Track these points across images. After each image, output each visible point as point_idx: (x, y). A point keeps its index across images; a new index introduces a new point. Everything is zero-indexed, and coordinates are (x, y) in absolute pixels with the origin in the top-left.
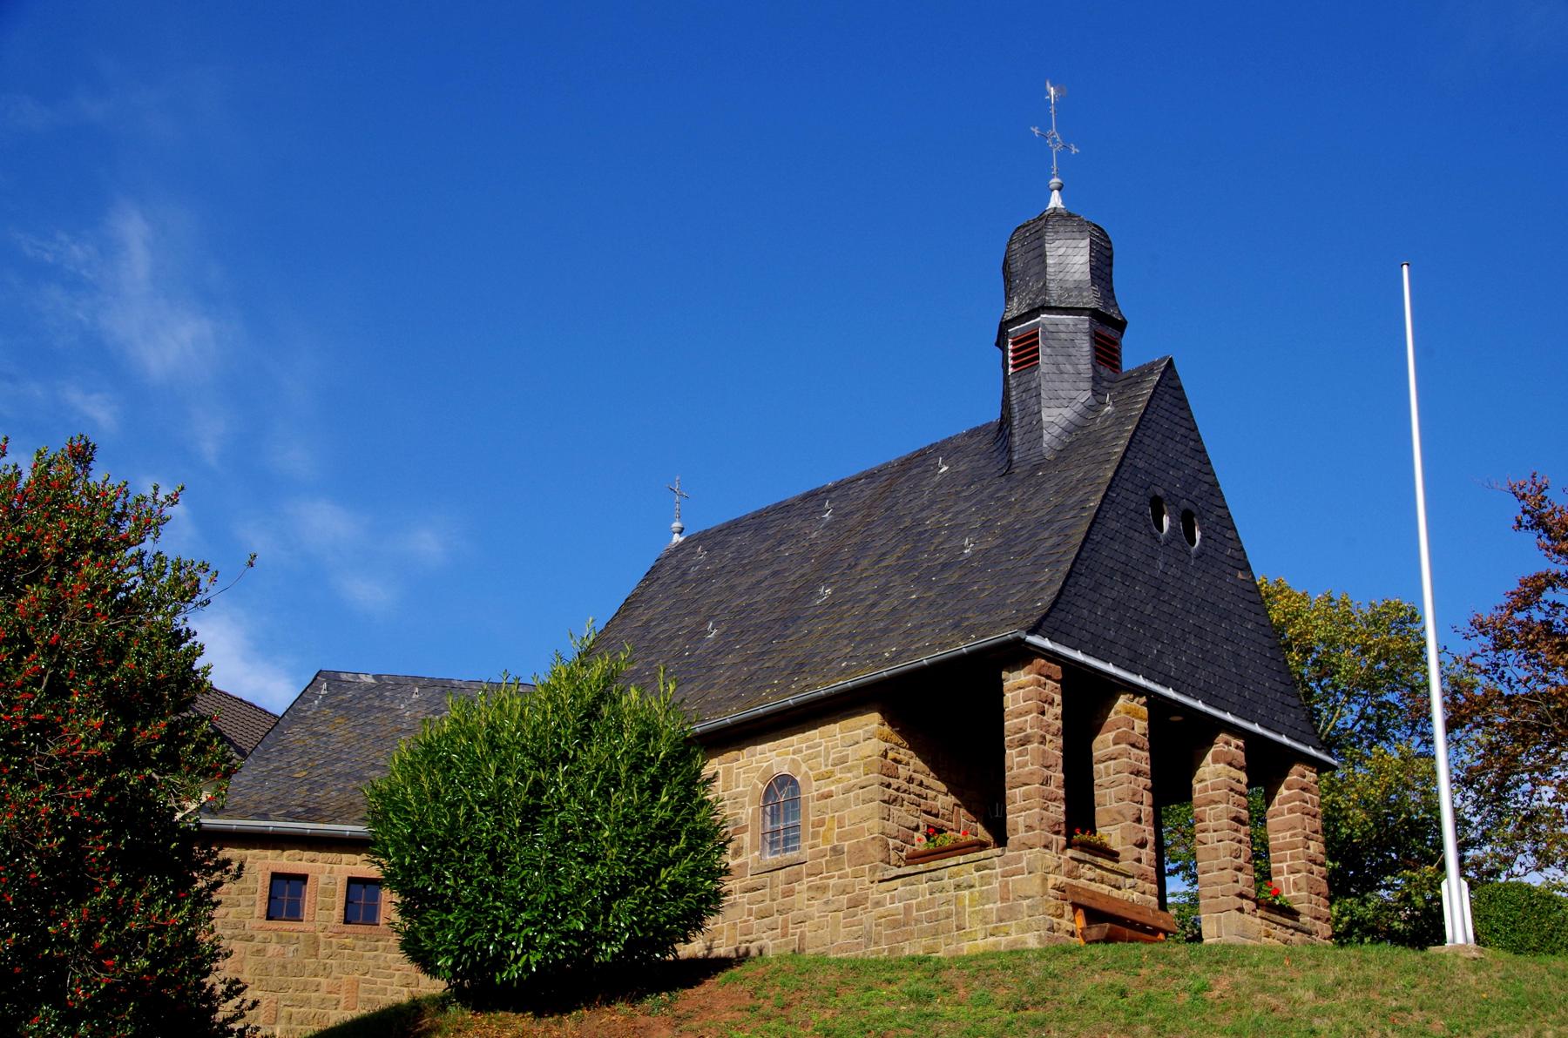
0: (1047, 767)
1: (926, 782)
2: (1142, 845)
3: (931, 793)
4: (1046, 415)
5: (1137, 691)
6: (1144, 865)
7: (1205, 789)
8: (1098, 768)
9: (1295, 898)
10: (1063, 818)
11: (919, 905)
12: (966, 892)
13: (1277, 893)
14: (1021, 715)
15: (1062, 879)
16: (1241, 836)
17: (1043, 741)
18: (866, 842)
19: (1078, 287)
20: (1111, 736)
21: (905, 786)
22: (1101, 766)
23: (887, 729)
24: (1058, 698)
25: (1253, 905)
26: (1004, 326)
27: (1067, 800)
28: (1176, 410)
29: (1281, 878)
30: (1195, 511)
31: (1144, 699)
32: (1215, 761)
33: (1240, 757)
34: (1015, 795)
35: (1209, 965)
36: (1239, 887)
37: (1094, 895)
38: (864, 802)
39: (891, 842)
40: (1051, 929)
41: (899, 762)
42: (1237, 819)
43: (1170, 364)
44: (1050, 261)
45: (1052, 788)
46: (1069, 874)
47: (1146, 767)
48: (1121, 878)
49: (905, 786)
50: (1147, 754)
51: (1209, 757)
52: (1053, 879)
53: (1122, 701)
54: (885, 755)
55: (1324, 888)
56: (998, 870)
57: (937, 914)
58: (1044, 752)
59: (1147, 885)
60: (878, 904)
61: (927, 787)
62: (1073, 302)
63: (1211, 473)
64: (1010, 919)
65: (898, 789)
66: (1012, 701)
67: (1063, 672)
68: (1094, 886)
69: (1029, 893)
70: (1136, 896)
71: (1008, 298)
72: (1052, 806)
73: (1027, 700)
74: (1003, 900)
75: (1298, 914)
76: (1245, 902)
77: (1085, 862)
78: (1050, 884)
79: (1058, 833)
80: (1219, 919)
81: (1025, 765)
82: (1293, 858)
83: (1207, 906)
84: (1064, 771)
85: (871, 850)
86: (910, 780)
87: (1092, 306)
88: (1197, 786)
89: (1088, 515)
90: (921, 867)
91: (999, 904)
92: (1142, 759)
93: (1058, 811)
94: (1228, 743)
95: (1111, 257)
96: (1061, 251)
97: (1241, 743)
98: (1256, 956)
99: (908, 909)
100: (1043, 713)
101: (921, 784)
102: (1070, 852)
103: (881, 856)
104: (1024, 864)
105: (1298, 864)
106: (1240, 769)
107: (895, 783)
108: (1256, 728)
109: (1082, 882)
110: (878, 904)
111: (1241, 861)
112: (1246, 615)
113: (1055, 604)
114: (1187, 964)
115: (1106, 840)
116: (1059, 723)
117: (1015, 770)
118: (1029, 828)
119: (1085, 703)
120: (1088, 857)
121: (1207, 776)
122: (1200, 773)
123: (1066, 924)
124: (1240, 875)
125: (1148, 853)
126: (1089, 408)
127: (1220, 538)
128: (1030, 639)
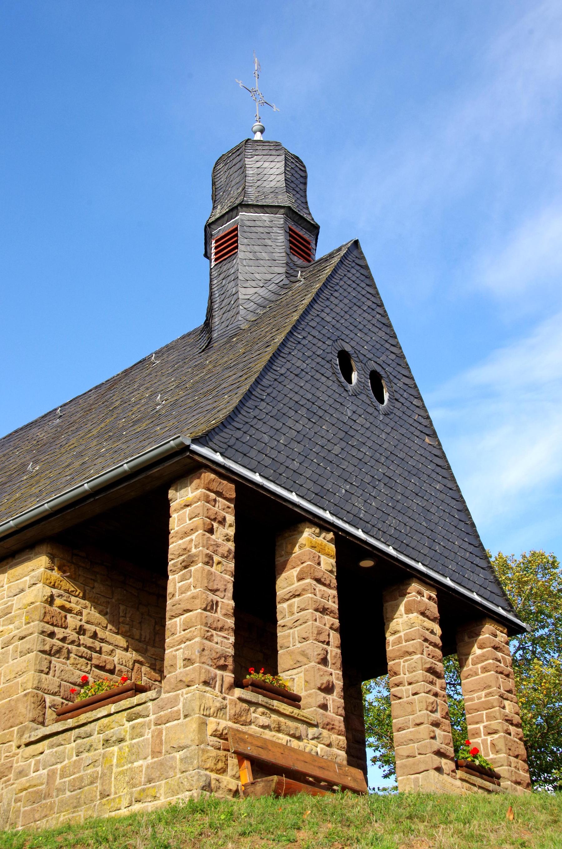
0: (214, 591)
1: (100, 634)
2: (328, 689)
3: (106, 648)
4: (243, 293)
5: (324, 526)
6: (330, 713)
7: (399, 641)
8: (282, 607)
9: (494, 761)
10: (231, 651)
11: (63, 770)
12: (115, 749)
13: (475, 752)
14: (186, 534)
15: (225, 724)
16: (437, 689)
17: (209, 561)
18: (18, 700)
19: (274, 192)
20: (295, 572)
21: (73, 636)
22: (285, 605)
23: (56, 574)
24: (231, 518)
25: (453, 766)
26: (209, 227)
27: (237, 631)
28: (363, 285)
29: (479, 740)
30: (382, 373)
31: (331, 535)
32: (408, 611)
33: (434, 609)
34: (175, 625)
35: (397, 821)
36: (437, 744)
37: (265, 745)
38: (22, 654)
39: (49, 699)
40: (207, 787)
41: (69, 611)
42: (431, 670)
43: (356, 243)
44: (249, 172)
45: (219, 615)
46: (236, 719)
47: (334, 606)
48: (302, 728)
49: (73, 636)
50: (335, 592)
51: (402, 608)
52: (212, 724)
53: (308, 534)
54: (51, 600)
55: (522, 750)
56: (152, 717)
57: (81, 779)
58: (210, 573)
59: (334, 737)
60: (21, 773)
61: (102, 640)
62: (269, 201)
63: (397, 346)
64: (159, 779)
65: (63, 640)
66: (178, 521)
67: (237, 491)
68: (268, 735)
69: (183, 742)
70: (320, 748)
71: (214, 208)
72: (217, 637)
73: (197, 527)
74: (155, 753)
75: (498, 777)
76: (444, 761)
77: (257, 705)
78: (210, 729)
79: (223, 668)
80: (417, 780)
81: (188, 588)
82: (489, 718)
83: (404, 766)
84: (235, 597)
85: (22, 709)
86: (81, 631)
87: (287, 204)
88: (390, 638)
89: (271, 350)
90: (70, 723)
91: (150, 760)
92: (330, 597)
93: (225, 643)
94: (420, 593)
95: (305, 177)
96: (258, 165)
97: (434, 595)
98: (465, 808)
99: (51, 776)
100: (211, 531)
101: (94, 636)
102: (238, 692)
103: (31, 716)
104: (180, 706)
105: (495, 724)
106: (433, 620)
107: (60, 632)
108: (448, 581)
109: (253, 729)
110: (21, 773)
111: (437, 716)
112: (434, 475)
113: (230, 418)
114: (367, 820)
115: (288, 684)
116: (231, 545)
117: (177, 597)
118: (188, 661)
119: (262, 532)
120: (261, 699)
121: (400, 628)
122: (393, 625)
123: (229, 781)
124: (438, 731)
125: (335, 700)
126: (283, 287)
127: (407, 404)
128: (194, 447)
